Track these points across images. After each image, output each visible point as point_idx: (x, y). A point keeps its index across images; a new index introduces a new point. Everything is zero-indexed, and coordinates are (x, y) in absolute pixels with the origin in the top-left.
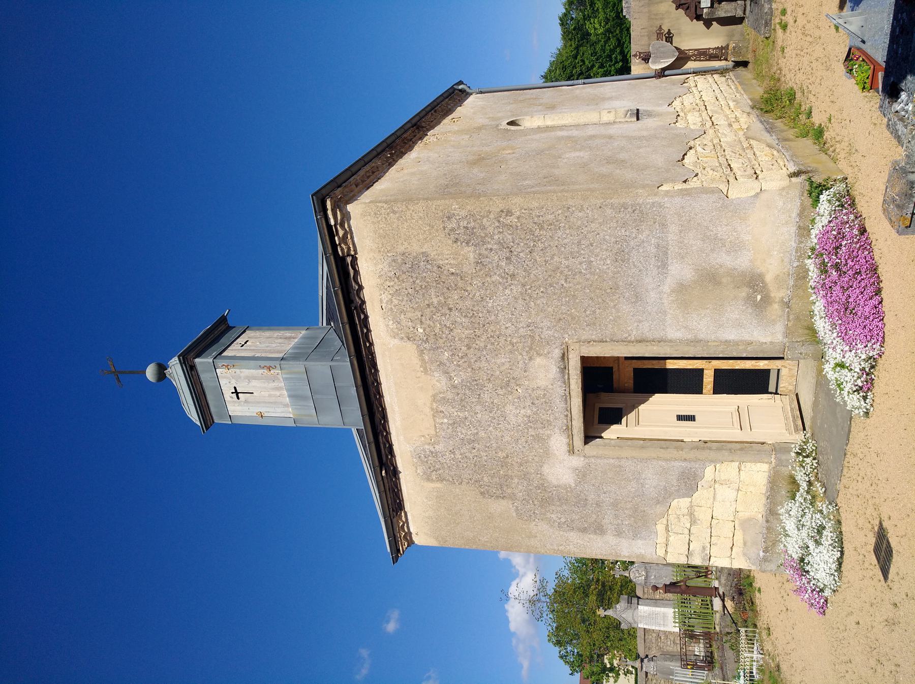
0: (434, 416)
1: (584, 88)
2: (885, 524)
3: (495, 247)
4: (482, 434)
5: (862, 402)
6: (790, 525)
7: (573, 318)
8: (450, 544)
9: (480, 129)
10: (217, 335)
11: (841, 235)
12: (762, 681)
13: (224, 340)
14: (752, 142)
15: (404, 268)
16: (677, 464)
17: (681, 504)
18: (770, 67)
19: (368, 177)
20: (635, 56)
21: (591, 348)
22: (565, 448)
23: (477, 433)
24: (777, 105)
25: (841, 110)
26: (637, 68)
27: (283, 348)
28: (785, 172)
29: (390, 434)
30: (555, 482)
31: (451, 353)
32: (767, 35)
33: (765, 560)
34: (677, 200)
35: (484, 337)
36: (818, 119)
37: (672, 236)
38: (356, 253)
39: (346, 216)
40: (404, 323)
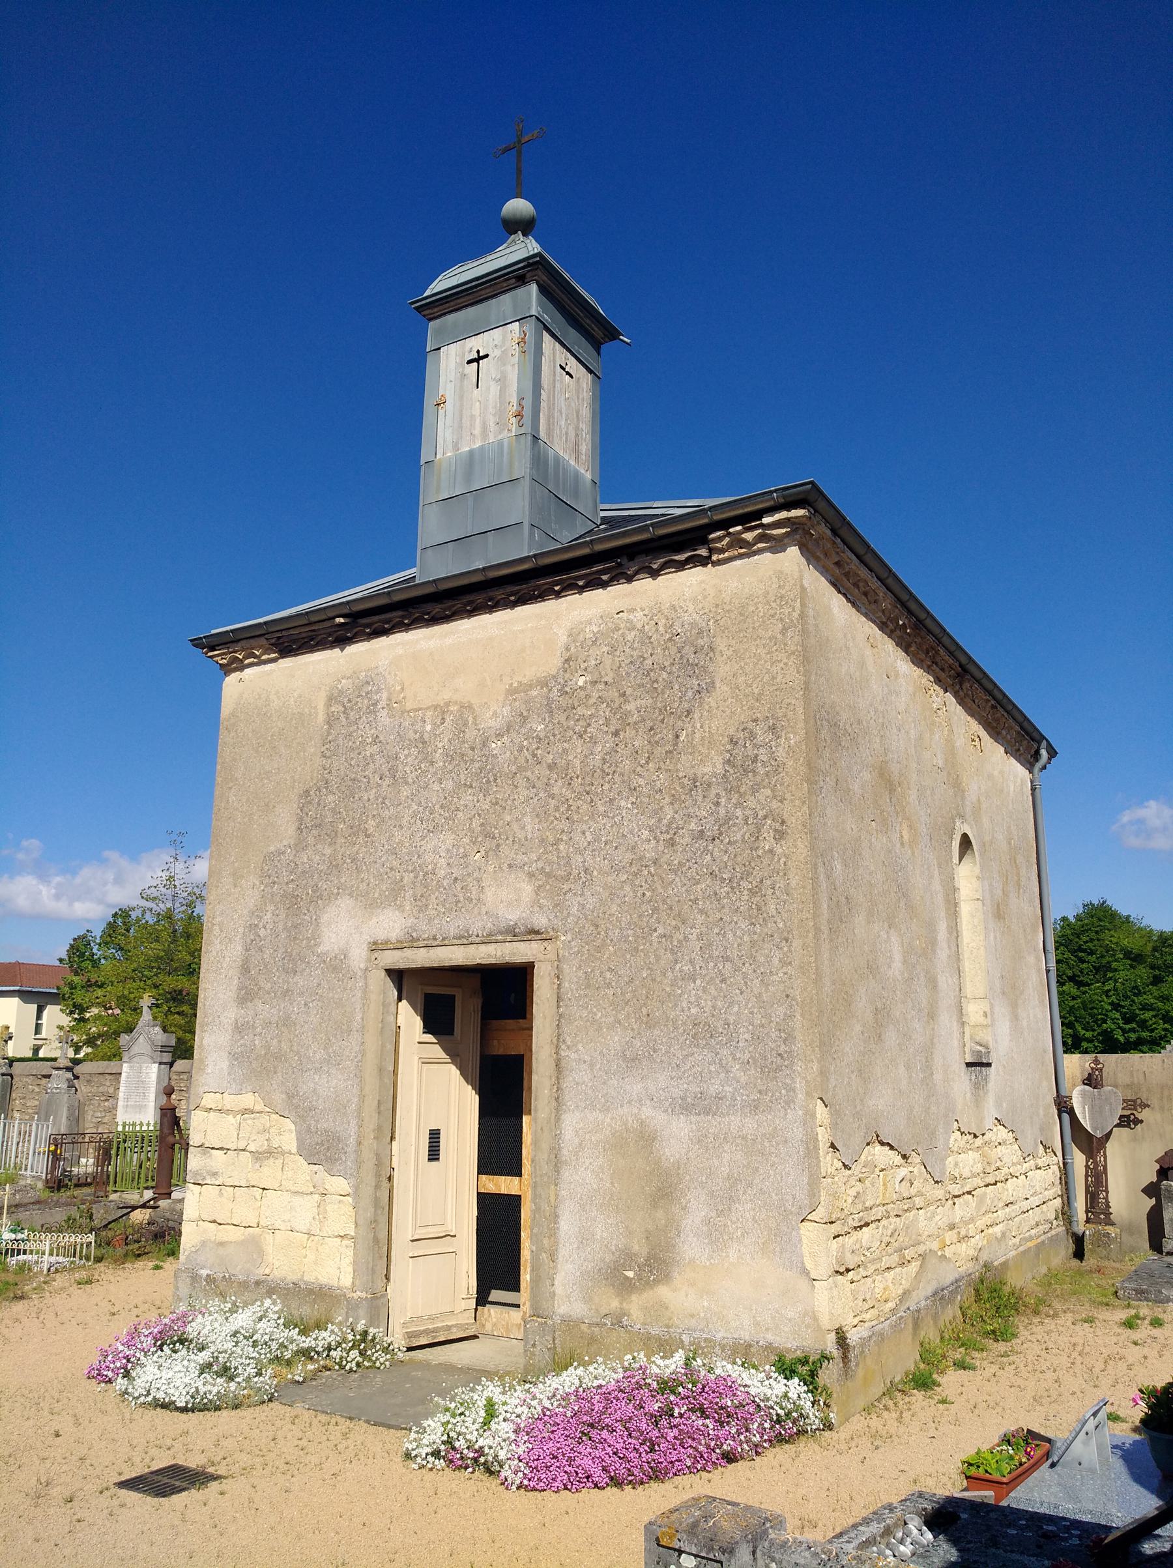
0: (436, 707)
1: (1039, 970)
2: (214, 1486)
3: (722, 811)
4: (406, 792)
5: (429, 1450)
6: (243, 1319)
7: (598, 949)
8: (225, 737)
9: (957, 785)
10: (582, 323)
11: (724, 1417)
12: (5, 1270)
13: (573, 335)
14: (915, 1265)
15: (688, 650)
16: (353, 1130)
17: (287, 1135)
18: (1062, 1297)
19: (856, 585)
20: (1096, 1061)
21: (547, 980)
22: (381, 936)
23: (406, 783)
24: (990, 1307)
25: (956, 1422)
26: (1075, 1064)
27: (556, 439)
28: (848, 1321)
29: (407, 630)
30: (325, 918)
31: (542, 735)
32: (1121, 1293)
33: (195, 1278)
34: (798, 1133)
35: (568, 794)
36: (950, 1380)
37: (736, 1122)
38: (715, 564)
39: (778, 546)
40: (595, 652)
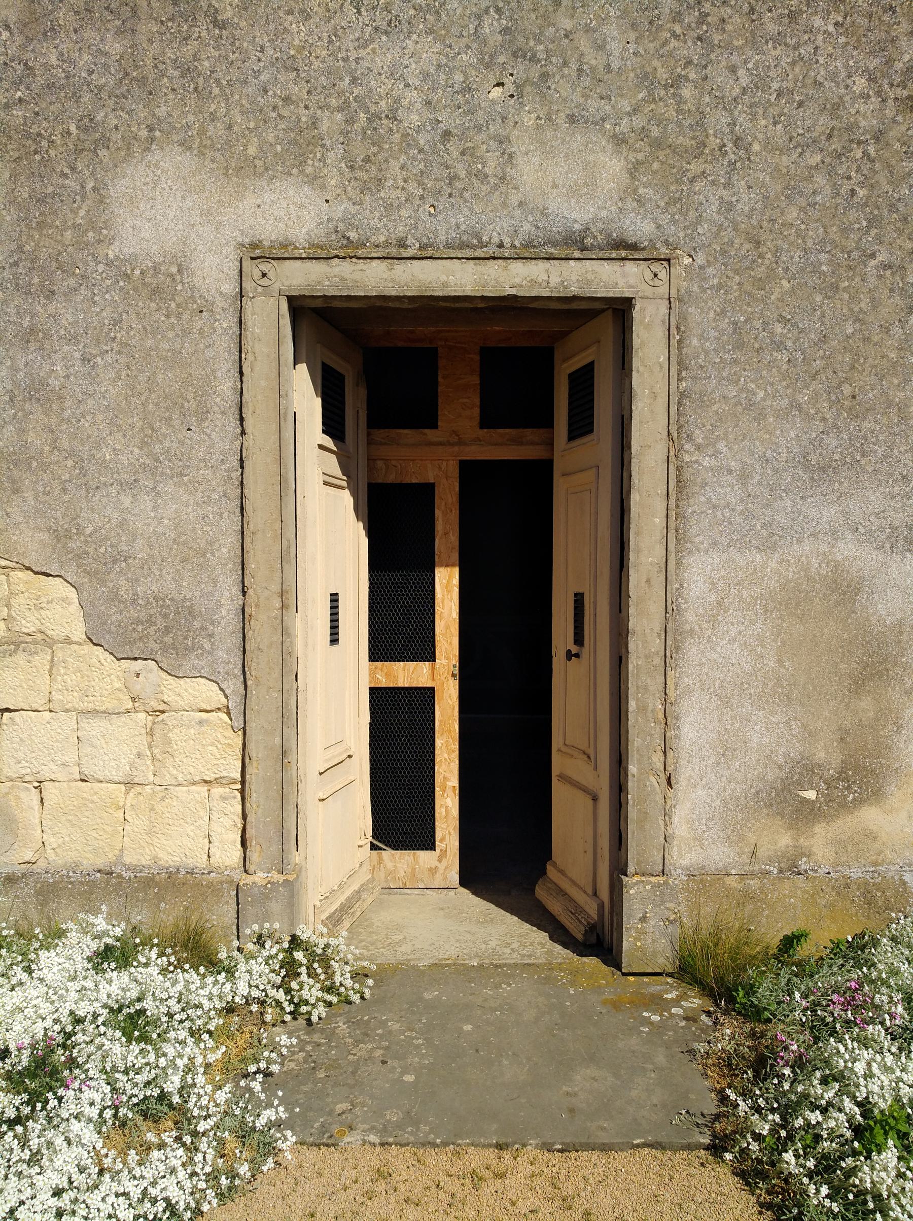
7: (760, 284)
22: (269, 231)
30: (119, 188)
